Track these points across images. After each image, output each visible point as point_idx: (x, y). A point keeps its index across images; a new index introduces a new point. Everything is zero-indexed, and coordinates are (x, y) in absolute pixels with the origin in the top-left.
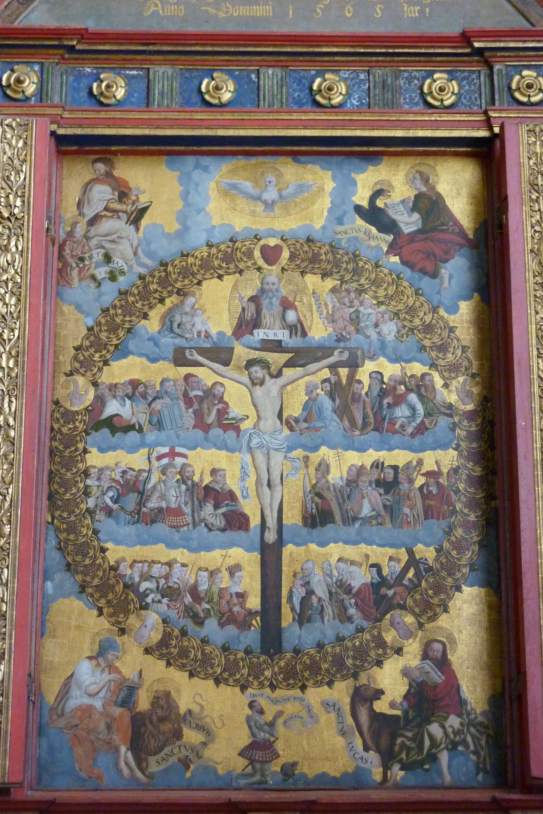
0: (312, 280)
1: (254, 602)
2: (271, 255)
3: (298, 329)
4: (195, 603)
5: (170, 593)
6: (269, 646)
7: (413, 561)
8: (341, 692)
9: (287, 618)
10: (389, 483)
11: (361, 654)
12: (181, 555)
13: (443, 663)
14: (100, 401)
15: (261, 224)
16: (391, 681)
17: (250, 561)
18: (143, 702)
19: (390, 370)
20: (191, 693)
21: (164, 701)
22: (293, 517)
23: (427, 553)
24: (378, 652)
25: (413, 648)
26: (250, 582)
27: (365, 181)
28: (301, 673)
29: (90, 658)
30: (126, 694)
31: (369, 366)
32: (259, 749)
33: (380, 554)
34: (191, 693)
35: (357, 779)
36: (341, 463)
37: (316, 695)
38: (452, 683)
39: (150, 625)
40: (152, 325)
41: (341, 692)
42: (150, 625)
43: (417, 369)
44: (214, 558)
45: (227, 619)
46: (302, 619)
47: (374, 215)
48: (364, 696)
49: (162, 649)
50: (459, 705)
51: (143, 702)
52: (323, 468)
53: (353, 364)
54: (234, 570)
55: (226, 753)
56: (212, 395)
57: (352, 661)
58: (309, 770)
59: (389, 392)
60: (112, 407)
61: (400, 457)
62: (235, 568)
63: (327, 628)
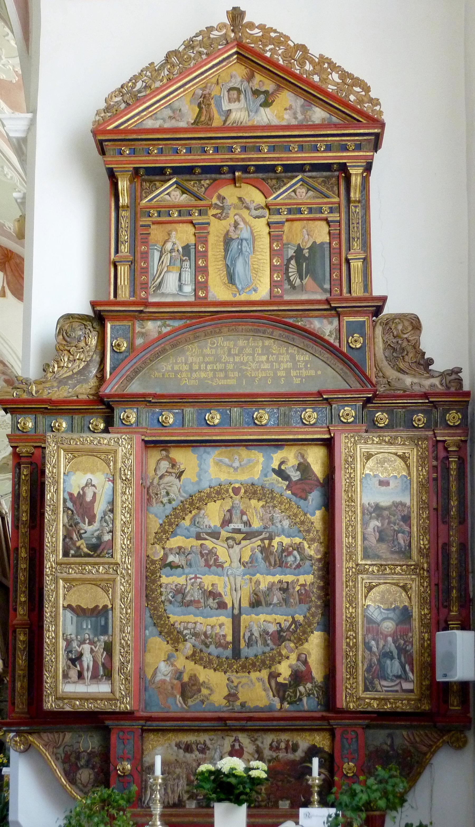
0: (254, 502)
1: (229, 638)
2: (236, 491)
3: (247, 524)
4: (205, 639)
5: (196, 635)
6: (235, 656)
7: (294, 621)
8: (264, 674)
9: (243, 644)
10: (285, 589)
11: (273, 659)
12: (200, 619)
13: (305, 663)
14: (166, 555)
15: (232, 478)
16: (284, 670)
17: (227, 622)
18: (186, 678)
19: (286, 541)
20: (204, 675)
21: (194, 678)
22: (245, 604)
23: (300, 618)
24: (277, 658)
25: (293, 656)
26: (228, 631)
27: (277, 457)
28: (249, 666)
29: (236, 15)
30: (179, 675)
31: (277, 539)
32: (232, 696)
33: (280, 618)
34: (204, 675)
35: (270, 708)
36: (265, 581)
37: (254, 675)
38: (309, 672)
39: (188, 648)
40: (187, 523)
41: (264, 674)
42: (188, 648)
43: (297, 540)
44: (213, 620)
45: (219, 645)
46: (249, 645)
47: (280, 473)
48: (273, 676)
49: (193, 657)
50: (311, 679)
51: (186, 678)
52: (258, 583)
53: (271, 539)
54: (221, 626)
55: (218, 698)
56: (212, 552)
57: (268, 662)
58: (251, 704)
59: (285, 551)
60: (171, 558)
61: (289, 578)
62: (221, 624)
63: (259, 648)
